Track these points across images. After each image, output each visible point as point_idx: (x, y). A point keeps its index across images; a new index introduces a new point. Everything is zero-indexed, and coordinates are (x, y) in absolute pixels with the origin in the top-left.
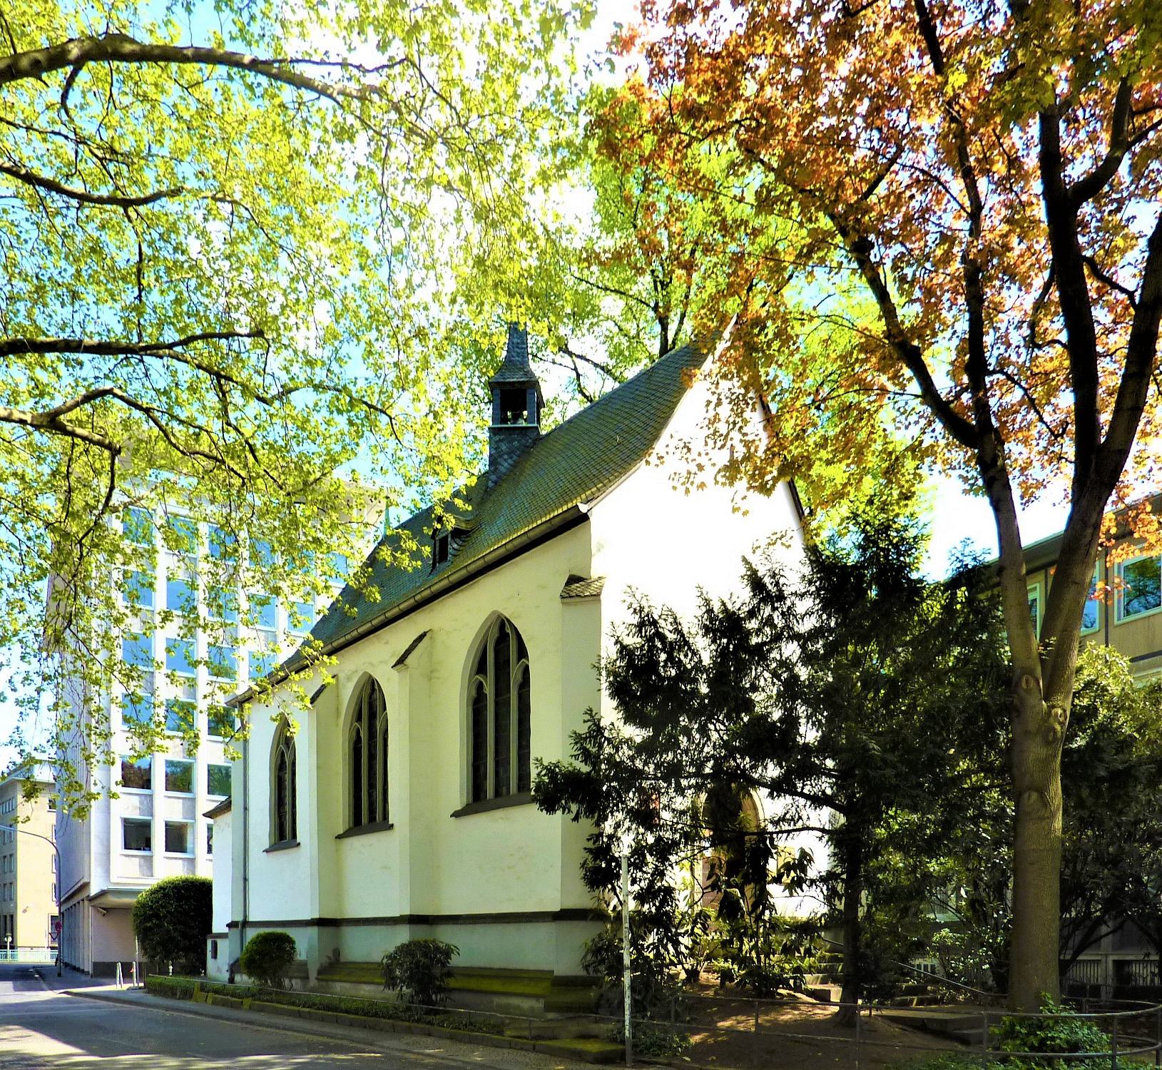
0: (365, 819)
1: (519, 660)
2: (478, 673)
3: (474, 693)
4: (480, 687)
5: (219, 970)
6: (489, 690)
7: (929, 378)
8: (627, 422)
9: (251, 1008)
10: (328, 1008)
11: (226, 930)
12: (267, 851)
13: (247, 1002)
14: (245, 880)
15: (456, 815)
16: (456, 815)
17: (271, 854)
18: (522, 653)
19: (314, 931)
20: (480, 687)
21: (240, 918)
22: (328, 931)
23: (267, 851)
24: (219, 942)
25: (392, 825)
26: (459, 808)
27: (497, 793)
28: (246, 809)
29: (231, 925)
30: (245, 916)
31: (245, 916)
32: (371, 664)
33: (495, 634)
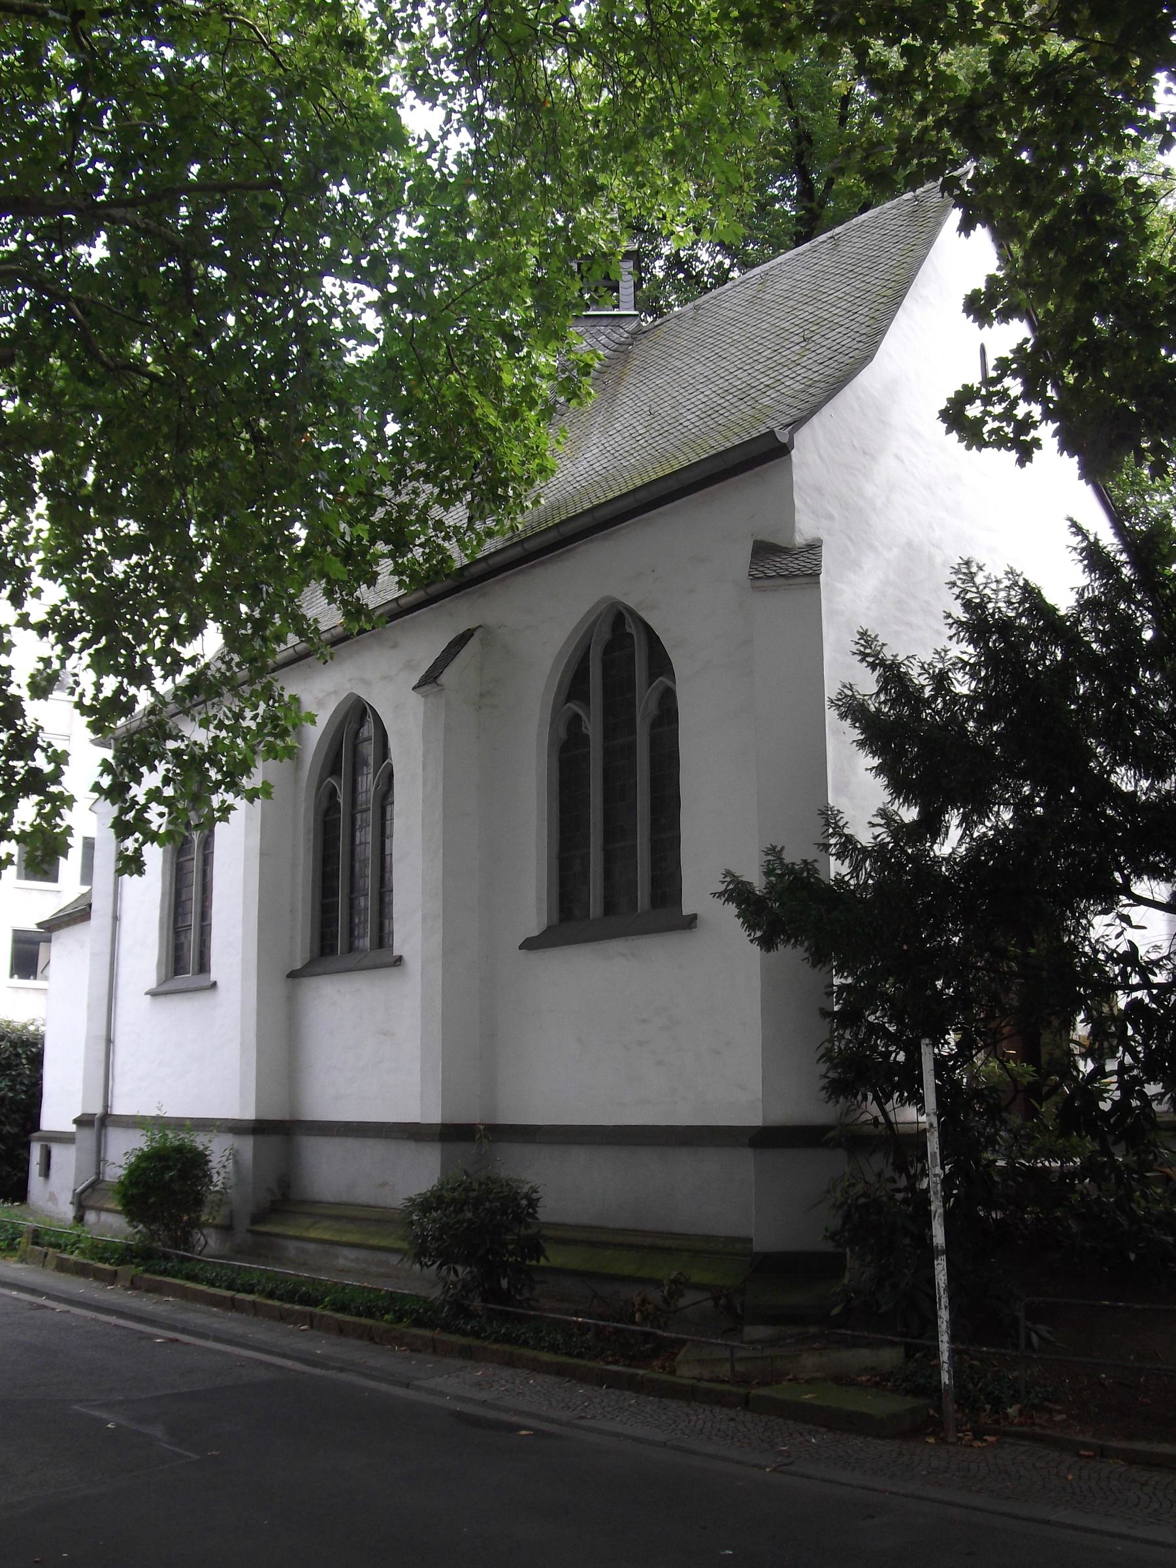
0: (596, 907)
1: (652, 677)
2: (569, 699)
3: (562, 733)
4: (575, 722)
5: (53, 1198)
6: (593, 728)
7: (695, 491)
8: (810, 309)
9: (134, 1285)
10: (290, 1297)
11: (73, 1128)
12: (154, 994)
13: (131, 1270)
14: (109, 1041)
15: (529, 945)
16: (529, 945)
17: (162, 1000)
18: (660, 663)
19: (745, 1162)
20: (575, 722)
21: (98, 1110)
22: (274, 1141)
23: (154, 994)
24: (57, 1151)
25: (400, 959)
26: (536, 933)
27: (609, 907)
28: (116, 918)
29: (82, 1122)
30: (106, 1106)
31: (106, 1106)
32: (364, 681)
33: (604, 633)
